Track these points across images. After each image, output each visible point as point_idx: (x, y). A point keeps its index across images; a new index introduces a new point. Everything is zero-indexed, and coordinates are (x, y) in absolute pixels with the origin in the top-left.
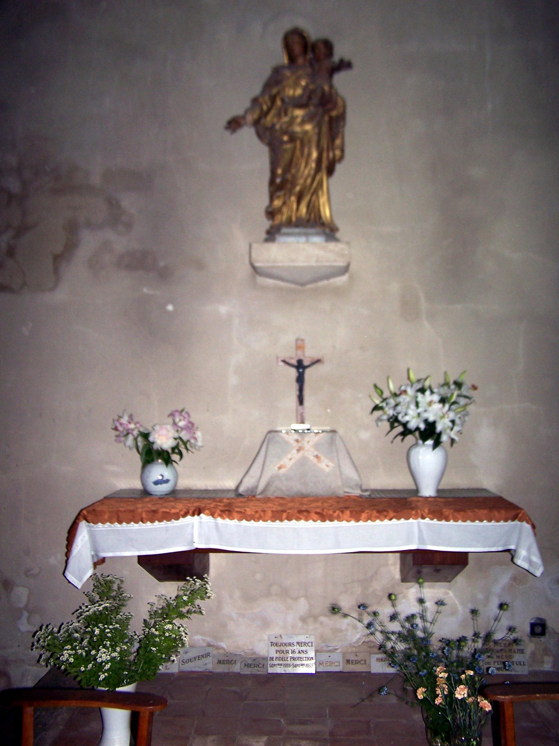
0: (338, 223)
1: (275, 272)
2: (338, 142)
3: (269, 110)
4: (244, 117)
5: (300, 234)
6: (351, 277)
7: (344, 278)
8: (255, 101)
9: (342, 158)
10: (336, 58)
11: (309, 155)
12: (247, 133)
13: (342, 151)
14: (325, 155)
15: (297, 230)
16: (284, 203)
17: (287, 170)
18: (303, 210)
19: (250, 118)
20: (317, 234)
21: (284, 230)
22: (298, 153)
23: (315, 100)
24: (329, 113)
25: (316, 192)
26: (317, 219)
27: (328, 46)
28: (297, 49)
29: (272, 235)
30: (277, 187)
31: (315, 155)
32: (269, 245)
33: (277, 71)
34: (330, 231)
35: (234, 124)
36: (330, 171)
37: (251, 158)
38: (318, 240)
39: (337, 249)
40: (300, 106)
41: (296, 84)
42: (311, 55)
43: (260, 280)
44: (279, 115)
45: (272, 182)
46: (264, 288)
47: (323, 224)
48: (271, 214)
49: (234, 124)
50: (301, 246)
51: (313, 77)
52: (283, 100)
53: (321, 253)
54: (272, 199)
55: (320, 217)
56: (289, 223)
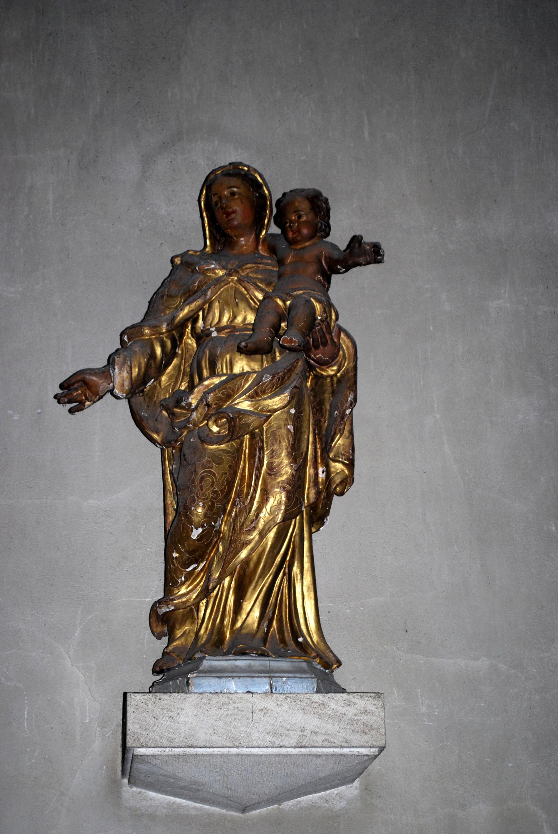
0: (338, 646)
1: (187, 773)
2: (339, 442)
3: (168, 357)
4: (105, 372)
5: (250, 673)
6: (366, 789)
7: (351, 791)
8: (131, 333)
9: (348, 481)
10: (339, 237)
11: (272, 471)
12: (111, 415)
13: (351, 465)
14: (309, 471)
15: (241, 662)
16: (206, 593)
17: (215, 511)
18: (252, 613)
19: (121, 377)
20: (295, 672)
21: (209, 662)
22: (244, 465)
23: (294, 338)
24: (318, 374)
25: (285, 567)
26: (288, 635)
27: (318, 205)
28: (239, 212)
29: (171, 673)
30: (186, 548)
31: (286, 470)
32: (167, 699)
33: (184, 264)
34: (322, 667)
35: (77, 391)
36: (318, 516)
37: (116, 478)
38: (303, 687)
39: (351, 712)
40: (248, 352)
41: (234, 301)
42: (264, 226)
43: (130, 792)
44: (194, 375)
45: (174, 536)
46: (138, 815)
47: (304, 648)
48: (163, 620)
49: (77, 391)
50: (260, 702)
51: (278, 282)
52: (201, 337)
53: (311, 722)
54: (170, 583)
55: (296, 632)
56: (217, 644)
